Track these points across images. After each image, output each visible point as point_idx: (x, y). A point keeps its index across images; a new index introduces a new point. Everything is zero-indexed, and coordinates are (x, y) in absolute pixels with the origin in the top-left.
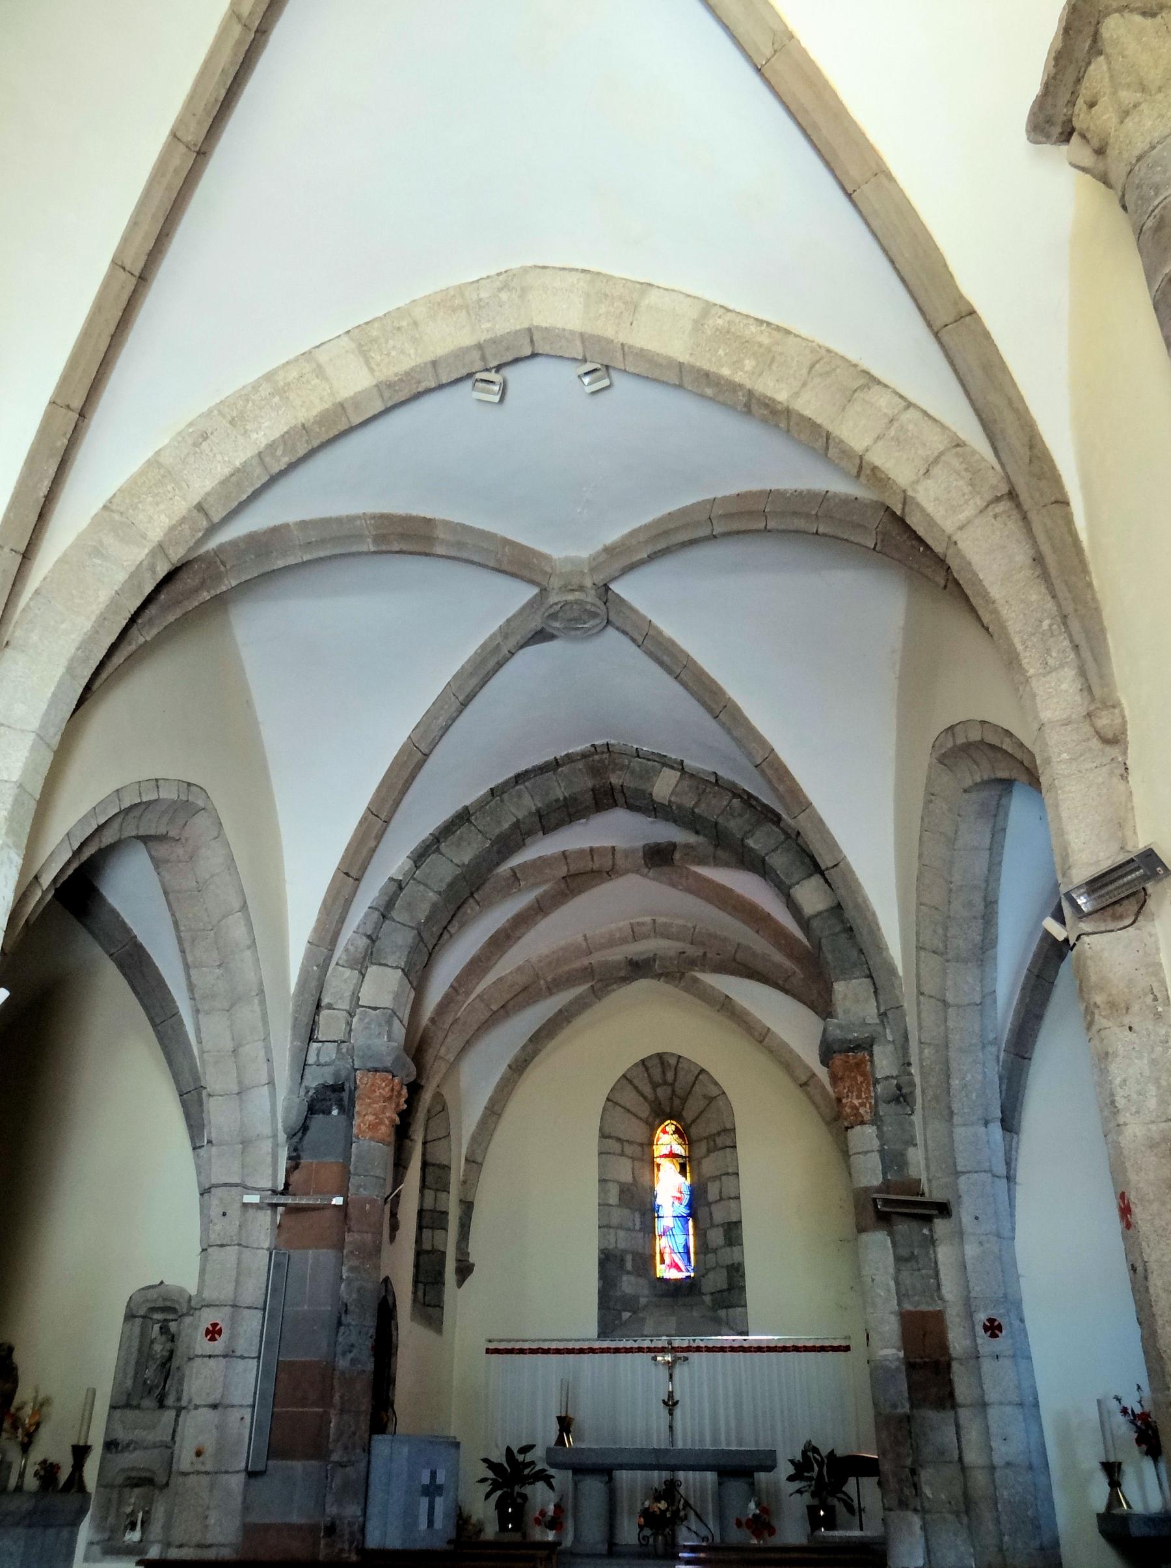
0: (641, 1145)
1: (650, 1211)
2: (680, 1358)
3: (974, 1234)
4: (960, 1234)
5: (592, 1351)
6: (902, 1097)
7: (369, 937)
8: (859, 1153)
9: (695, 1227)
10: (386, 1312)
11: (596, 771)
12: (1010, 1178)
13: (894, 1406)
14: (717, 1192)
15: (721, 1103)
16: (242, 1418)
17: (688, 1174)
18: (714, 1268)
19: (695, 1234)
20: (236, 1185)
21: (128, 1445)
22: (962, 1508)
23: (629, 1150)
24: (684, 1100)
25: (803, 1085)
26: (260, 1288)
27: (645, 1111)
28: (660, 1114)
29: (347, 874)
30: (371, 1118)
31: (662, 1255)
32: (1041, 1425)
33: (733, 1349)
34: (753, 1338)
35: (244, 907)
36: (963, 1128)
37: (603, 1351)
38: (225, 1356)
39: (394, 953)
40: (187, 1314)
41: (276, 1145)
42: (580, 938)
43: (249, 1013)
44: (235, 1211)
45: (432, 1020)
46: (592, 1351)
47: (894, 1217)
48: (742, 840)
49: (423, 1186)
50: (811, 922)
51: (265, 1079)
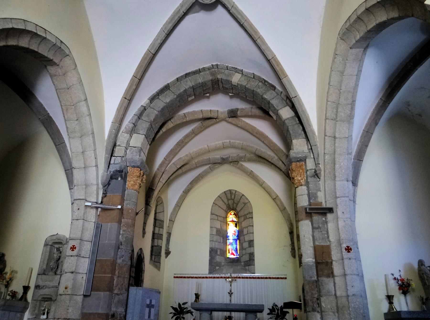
0: (224, 218)
1: (225, 237)
2: (234, 280)
3: (342, 218)
4: (337, 218)
5: (207, 278)
6: (316, 175)
7: (134, 124)
8: (300, 195)
9: (239, 242)
10: (140, 259)
11: (212, 74)
12: (354, 202)
13: (311, 277)
14: (247, 231)
15: (249, 205)
16: (83, 277)
17: (238, 227)
18: (245, 254)
19: (239, 245)
20: (83, 199)
21: (43, 287)
22: (336, 310)
23: (219, 218)
24: (237, 204)
25: (274, 199)
26: (91, 235)
27: (225, 207)
28: (230, 208)
29: (125, 98)
30: (132, 182)
31: (229, 250)
32: (364, 283)
33: (250, 278)
34: (256, 275)
35: (86, 100)
36: (340, 182)
37: (210, 278)
38: (77, 256)
39: (142, 130)
40: (66, 244)
41: (98, 188)
42: (206, 146)
43: (88, 140)
44: (82, 208)
45: (158, 169)
46: (207, 278)
47: (313, 214)
48: (262, 96)
49: (155, 226)
50: (285, 121)
51: (94, 165)
